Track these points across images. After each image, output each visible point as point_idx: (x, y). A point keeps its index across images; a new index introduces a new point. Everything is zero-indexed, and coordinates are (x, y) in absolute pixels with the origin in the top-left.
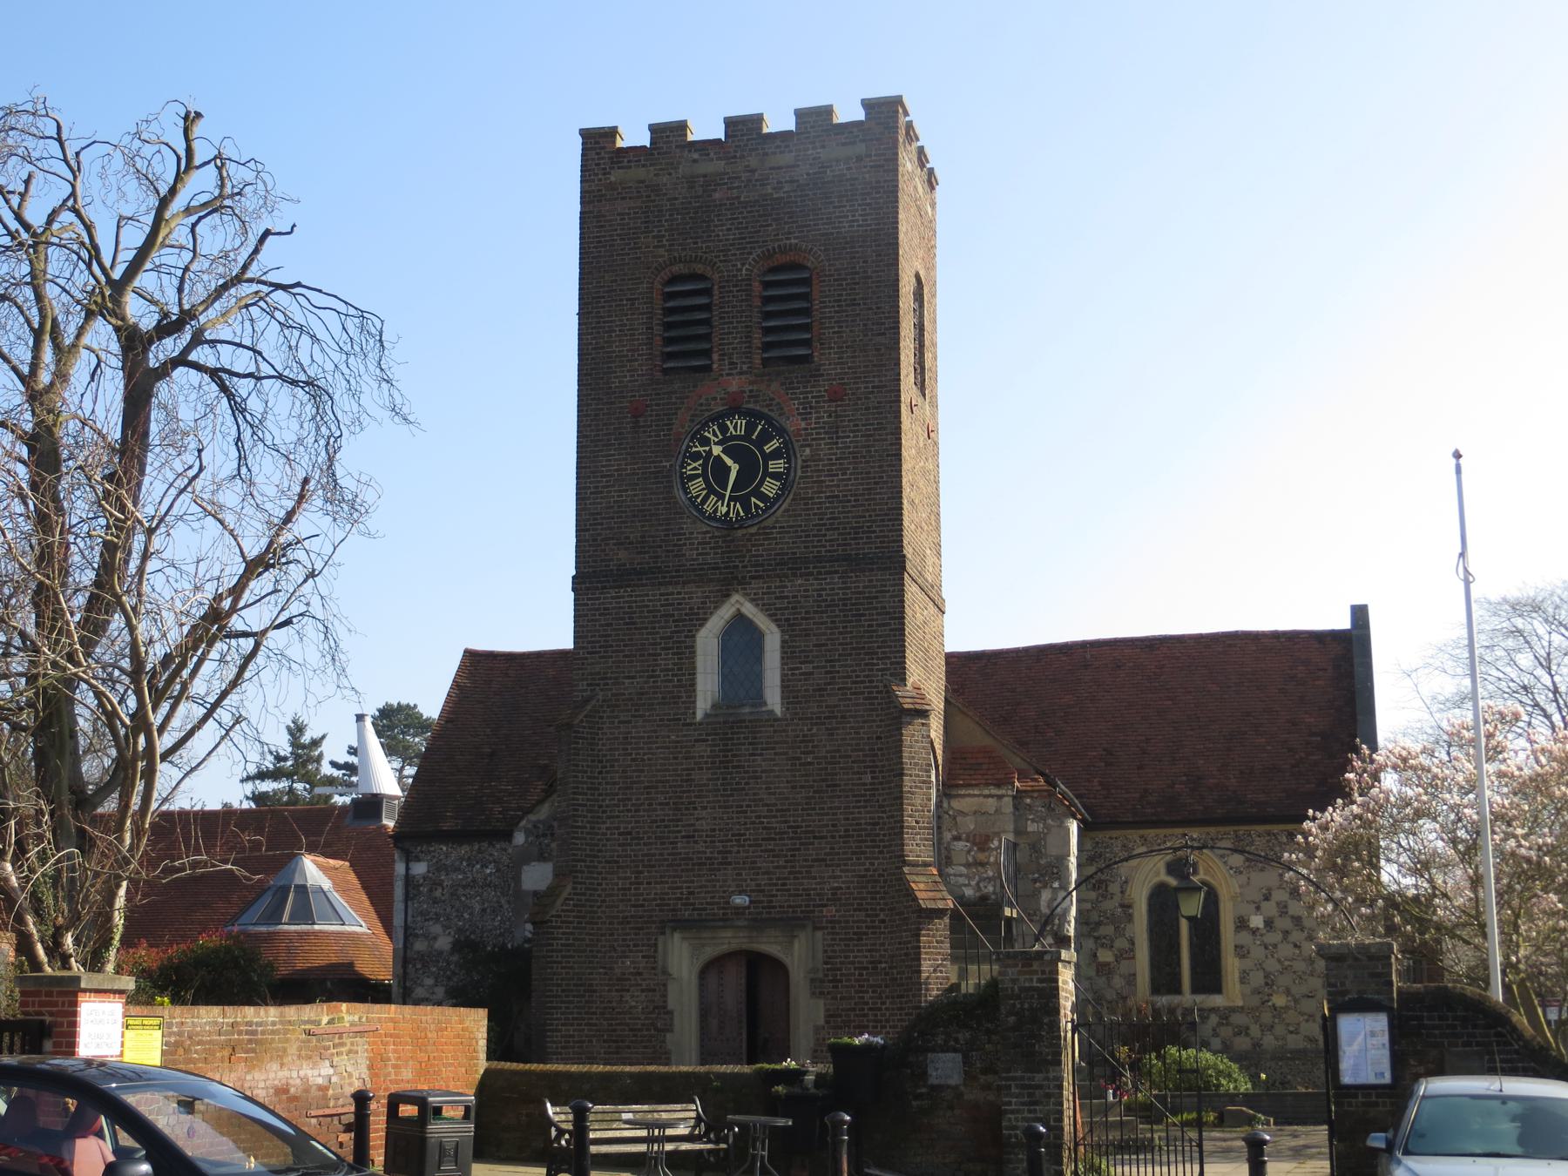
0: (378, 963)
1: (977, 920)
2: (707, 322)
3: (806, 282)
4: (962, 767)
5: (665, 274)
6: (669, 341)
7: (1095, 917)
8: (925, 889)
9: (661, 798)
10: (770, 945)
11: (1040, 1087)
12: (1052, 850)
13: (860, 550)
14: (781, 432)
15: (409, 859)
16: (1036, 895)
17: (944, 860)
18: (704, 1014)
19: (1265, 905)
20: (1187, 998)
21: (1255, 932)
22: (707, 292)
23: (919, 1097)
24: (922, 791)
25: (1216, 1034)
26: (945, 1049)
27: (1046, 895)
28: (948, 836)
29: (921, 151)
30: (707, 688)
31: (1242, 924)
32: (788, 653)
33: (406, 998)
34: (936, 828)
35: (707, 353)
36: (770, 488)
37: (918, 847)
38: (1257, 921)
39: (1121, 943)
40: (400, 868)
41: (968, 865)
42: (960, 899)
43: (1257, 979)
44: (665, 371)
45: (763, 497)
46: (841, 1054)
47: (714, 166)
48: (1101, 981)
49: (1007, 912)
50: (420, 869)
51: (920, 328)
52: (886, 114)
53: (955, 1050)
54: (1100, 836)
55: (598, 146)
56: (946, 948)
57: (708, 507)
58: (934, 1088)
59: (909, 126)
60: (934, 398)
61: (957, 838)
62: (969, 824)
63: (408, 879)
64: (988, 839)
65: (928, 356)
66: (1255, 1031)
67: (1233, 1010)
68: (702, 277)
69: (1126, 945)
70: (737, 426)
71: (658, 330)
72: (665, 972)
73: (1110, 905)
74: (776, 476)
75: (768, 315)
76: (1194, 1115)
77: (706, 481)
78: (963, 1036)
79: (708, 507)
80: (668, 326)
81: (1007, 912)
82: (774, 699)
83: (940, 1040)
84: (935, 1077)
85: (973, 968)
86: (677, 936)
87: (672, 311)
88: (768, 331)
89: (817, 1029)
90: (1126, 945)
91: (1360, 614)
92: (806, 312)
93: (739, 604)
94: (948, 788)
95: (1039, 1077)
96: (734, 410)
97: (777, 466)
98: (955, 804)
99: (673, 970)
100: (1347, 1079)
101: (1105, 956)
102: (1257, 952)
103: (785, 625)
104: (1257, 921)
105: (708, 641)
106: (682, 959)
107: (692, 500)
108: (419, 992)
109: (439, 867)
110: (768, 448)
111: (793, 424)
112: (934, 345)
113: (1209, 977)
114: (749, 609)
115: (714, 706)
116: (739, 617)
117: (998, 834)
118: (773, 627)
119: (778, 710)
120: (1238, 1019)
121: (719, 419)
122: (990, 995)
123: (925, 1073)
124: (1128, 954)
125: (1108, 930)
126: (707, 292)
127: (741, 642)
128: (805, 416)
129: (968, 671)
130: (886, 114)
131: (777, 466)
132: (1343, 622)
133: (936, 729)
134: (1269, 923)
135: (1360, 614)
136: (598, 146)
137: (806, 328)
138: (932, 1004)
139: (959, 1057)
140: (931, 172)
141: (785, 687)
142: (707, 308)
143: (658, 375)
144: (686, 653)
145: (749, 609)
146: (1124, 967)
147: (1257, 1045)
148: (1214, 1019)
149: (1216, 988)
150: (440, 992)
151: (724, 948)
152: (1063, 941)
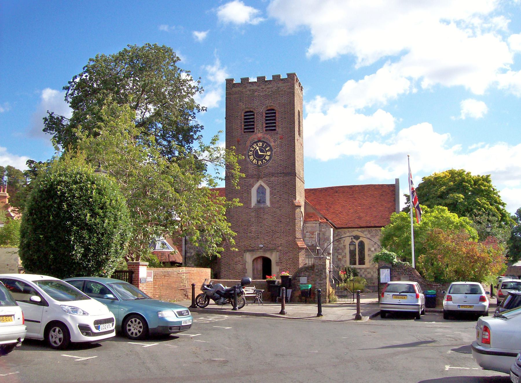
0: (180, 259)
1: (312, 249)
3: (275, 113)
4: (308, 217)
5: (244, 112)
6: (245, 126)
7: (338, 248)
8: (300, 244)
10: (267, 255)
12: (327, 234)
13: (287, 171)
14: (270, 146)
16: (324, 244)
17: (304, 237)
18: (253, 270)
20: (357, 266)
21: (372, 251)
24: (300, 223)
25: (363, 274)
27: (326, 245)
28: (305, 232)
29: (299, 83)
31: (369, 250)
32: (271, 193)
33: (186, 265)
34: (303, 231)
35: (253, 128)
37: (298, 235)
38: (373, 249)
39: (343, 254)
42: (308, 245)
44: (245, 132)
46: (283, 277)
47: (255, 87)
48: (339, 262)
49: (317, 248)
51: (299, 122)
52: (292, 77)
56: (304, 256)
59: (297, 79)
60: (302, 136)
62: (309, 229)
63: (186, 240)
64: (314, 232)
65: (301, 128)
66: (372, 273)
67: (368, 268)
68: (252, 112)
70: (260, 144)
71: (243, 123)
73: (341, 246)
75: (266, 120)
76: (377, 300)
78: (307, 274)
79: (254, 162)
81: (317, 248)
82: (268, 203)
85: (310, 260)
88: (267, 124)
89: (277, 273)
91: (397, 180)
92: (275, 120)
93: (260, 182)
94: (305, 222)
95: (322, 282)
96: (259, 141)
98: (307, 225)
100: (381, 282)
101: (340, 257)
103: (271, 187)
104: (373, 249)
105: (254, 191)
106: (249, 258)
108: (188, 265)
110: (267, 149)
111: (272, 144)
112: (302, 131)
114: (263, 184)
116: (261, 185)
117: (316, 231)
119: (269, 206)
120: (368, 270)
122: (312, 267)
125: (340, 251)
126: (254, 115)
127: (261, 191)
128: (274, 142)
129: (309, 192)
130: (292, 77)
132: (394, 183)
133: (302, 209)
135: (397, 180)
137: (275, 123)
138: (205, 31)
140: (302, 87)
142: (253, 118)
143: (243, 133)
145: (263, 184)
146: (344, 259)
148: (363, 270)
149: (364, 264)
150: (193, 265)
151: (258, 256)
152: (329, 254)
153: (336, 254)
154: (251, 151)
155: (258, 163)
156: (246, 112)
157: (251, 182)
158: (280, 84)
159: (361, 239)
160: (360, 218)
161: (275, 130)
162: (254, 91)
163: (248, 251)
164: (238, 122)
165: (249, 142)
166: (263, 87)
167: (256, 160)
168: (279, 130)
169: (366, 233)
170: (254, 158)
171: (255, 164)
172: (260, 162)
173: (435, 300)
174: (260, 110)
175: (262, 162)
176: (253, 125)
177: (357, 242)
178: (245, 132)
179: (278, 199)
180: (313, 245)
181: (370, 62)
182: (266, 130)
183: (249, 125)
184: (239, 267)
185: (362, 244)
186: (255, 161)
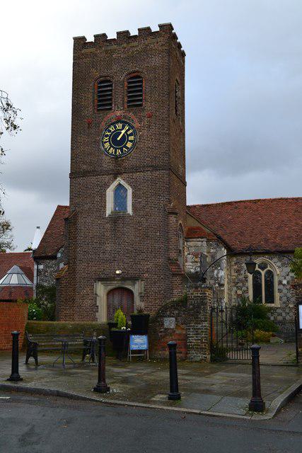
2: (111, 95)
9: (95, 241)
11: (199, 329)
14: (133, 127)
15: (38, 264)
19: (287, 277)
21: (284, 285)
22: (111, 86)
23: (161, 332)
26: (169, 316)
27: (216, 272)
30: (110, 208)
31: (280, 283)
32: (134, 196)
35: (111, 104)
36: (129, 145)
38: (285, 282)
39: (244, 288)
40: (36, 267)
41: (192, 262)
43: (285, 299)
45: (127, 148)
50: (41, 267)
53: (173, 317)
54: (81, 180)
55: (80, 43)
57: (110, 151)
58: (166, 329)
61: (189, 254)
62: (193, 250)
66: (284, 314)
68: (109, 81)
69: (246, 289)
72: (96, 294)
74: (131, 141)
77: (110, 144)
79: (110, 151)
80: (99, 101)
82: (130, 210)
83: (168, 313)
84: (166, 325)
86: (100, 283)
87: (100, 96)
90: (246, 289)
92: (141, 91)
93: (120, 180)
95: (199, 326)
96: (119, 121)
97: (131, 138)
99: (98, 293)
102: (285, 291)
103: (133, 187)
104: (285, 282)
105: (110, 193)
106: (101, 290)
107: (105, 149)
109: (46, 266)
111: (136, 125)
113: (270, 298)
114: (123, 182)
115: (112, 212)
116: (120, 184)
118: (130, 187)
120: (278, 311)
121: (114, 124)
123: (163, 324)
124: (247, 291)
125: (240, 284)
126: (111, 86)
128: (140, 122)
131: (131, 138)
134: (288, 282)
136: (80, 43)
137: (141, 96)
139: (174, 319)
141: (133, 206)
142: (111, 90)
144: (103, 196)
145: (123, 182)
147: (284, 319)
149: (273, 302)
153: (235, 289)
154: (107, 136)
155: (116, 152)
156: (101, 82)
157: (106, 180)
158: (150, 40)
159: (269, 268)
160: (267, 241)
161: (141, 105)
162: (112, 52)
163: (100, 279)
164: (90, 96)
165: (103, 123)
166: (125, 45)
167: (111, 145)
168: (148, 106)
169: (276, 260)
170: (111, 146)
171: (112, 154)
172: (119, 152)
173: (262, 411)
174: (120, 78)
175: (122, 152)
176: (111, 99)
177: (263, 273)
178: (98, 110)
179: (143, 203)
180: (197, 272)
181: (293, 368)
182: (129, 106)
183: (104, 102)
184: (88, 302)
185: (270, 274)
186: (112, 150)
